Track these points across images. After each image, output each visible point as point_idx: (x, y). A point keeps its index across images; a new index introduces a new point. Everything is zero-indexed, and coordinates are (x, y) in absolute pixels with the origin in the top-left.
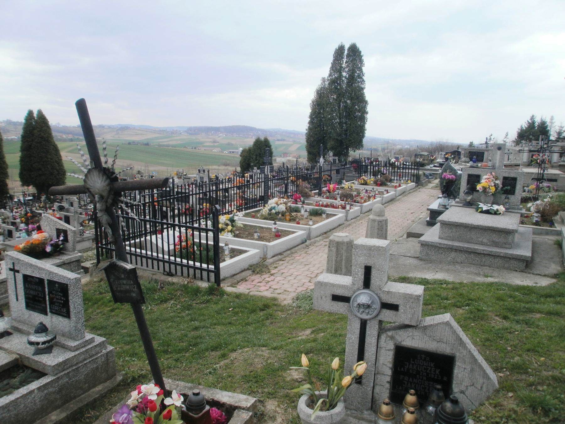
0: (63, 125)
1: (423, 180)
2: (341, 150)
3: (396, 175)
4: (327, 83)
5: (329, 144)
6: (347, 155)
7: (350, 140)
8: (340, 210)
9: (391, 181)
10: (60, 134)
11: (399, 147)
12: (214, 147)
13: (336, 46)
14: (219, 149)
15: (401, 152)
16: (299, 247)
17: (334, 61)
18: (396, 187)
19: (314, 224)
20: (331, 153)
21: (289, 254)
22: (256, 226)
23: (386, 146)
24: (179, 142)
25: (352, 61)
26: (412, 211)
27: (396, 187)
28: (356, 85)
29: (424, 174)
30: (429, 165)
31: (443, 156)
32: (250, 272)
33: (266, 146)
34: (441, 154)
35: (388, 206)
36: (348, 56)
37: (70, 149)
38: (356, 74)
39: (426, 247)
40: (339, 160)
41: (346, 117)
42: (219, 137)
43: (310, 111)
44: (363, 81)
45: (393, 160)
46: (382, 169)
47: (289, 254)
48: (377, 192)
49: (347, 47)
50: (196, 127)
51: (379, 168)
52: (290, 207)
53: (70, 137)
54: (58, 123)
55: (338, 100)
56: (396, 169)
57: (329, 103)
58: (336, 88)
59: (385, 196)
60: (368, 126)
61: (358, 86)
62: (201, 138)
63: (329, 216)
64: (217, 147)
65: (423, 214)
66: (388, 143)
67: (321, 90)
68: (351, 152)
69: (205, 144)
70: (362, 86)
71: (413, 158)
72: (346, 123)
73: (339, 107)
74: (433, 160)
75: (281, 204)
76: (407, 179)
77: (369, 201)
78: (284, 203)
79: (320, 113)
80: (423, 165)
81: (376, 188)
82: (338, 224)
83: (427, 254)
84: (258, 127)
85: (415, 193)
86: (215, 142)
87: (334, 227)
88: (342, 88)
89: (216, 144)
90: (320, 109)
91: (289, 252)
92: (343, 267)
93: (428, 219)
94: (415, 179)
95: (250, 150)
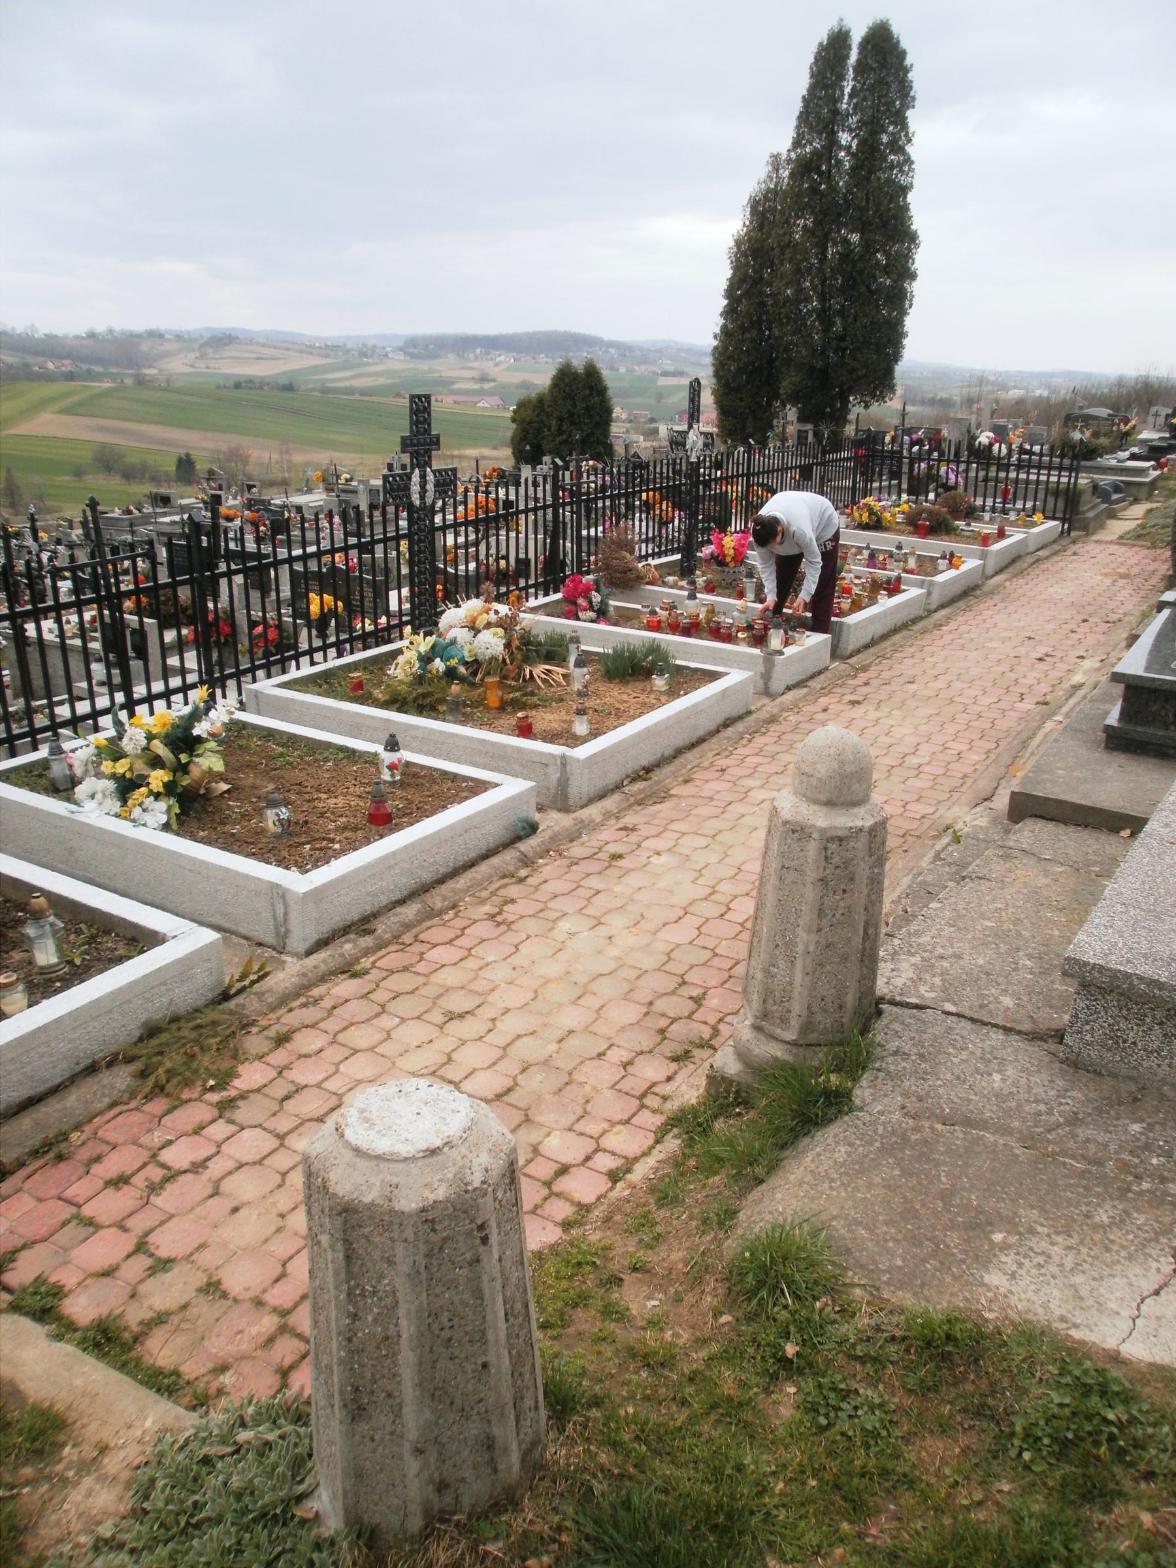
0: (48, 332)
1: (1090, 508)
2: (825, 400)
3: (990, 491)
4: (785, 174)
5: (785, 383)
6: (840, 418)
7: (853, 370)
8: (744, 649)
9: (971, 514)
10: (41, 360)
11: (1015, 394)
12: (482, 393)
13: (823, 37)
14: (496, 400)
15: (1019, 409)
16: (484, 868)
17: (812, 89)
18: (985, 540)
19: (594, 734)
20: (792, 413)
21: (408, 926)
22: (328, 745)
23: (974, 391)
24: (382, 381)
25: (871, 89)
26: (1041, 651)
27: (985, 540)
28: (883, 176)
29: (1095, 487)
30: (1112, 450)
31: (1161, 420)
32: (121, 1078)
33: (591, 388)
34: (1157, 415)
35: (948, 618)
36: (861, 68)
37: (67, 402)
38: (885, 138)
39: (1112, 1000)
40: (816, 434)
41: (842, 291)
42: (497, 365)
43: (729, 273)
44: (908, 161)
45: (984, 438)
46: (943, 469)
47: (408, 926)
48: (912, 563)
49: (857, 36)
50: (430, 337)
51: (930, 468)
52: (527, 640)
53: (68, 366)
54: (33, 327)
55: (820, 236)
56: (993, 468)
57: (788, 246)
58: (814, 190)
59: (940, 578)
60: (912, 322)
61: (890, 182)
62: (446, 367)
63: (686, 679)
64: (490, 393)
65: (1087, 664)
66: (982, 381)
67: (765, 196)
68: (856, 410)
69: (456, 386)
70: (903, 180)
71: (1055, 432)
72: (842, 313)
73: (823, 258)
74: (1127, 434)
75: (489, 625)
76: (1029, 505)
77: (873, 601)
78: (499, 624)
79: (758, 281)
80: (1089, 452)
81: (911, 541)
82: (719, 719)
83: (1116, 1040)
84: (607, 336)
85: (1059, 563)
86: (484, 379)
87: (701, 732)
88: (833, 189)
89: (487, 386)
90: (762, 266)
91: (410, 911)
92: (408, 1391)
93: (1113, 719)
94: (1061, 505)
95: (541, 400)
